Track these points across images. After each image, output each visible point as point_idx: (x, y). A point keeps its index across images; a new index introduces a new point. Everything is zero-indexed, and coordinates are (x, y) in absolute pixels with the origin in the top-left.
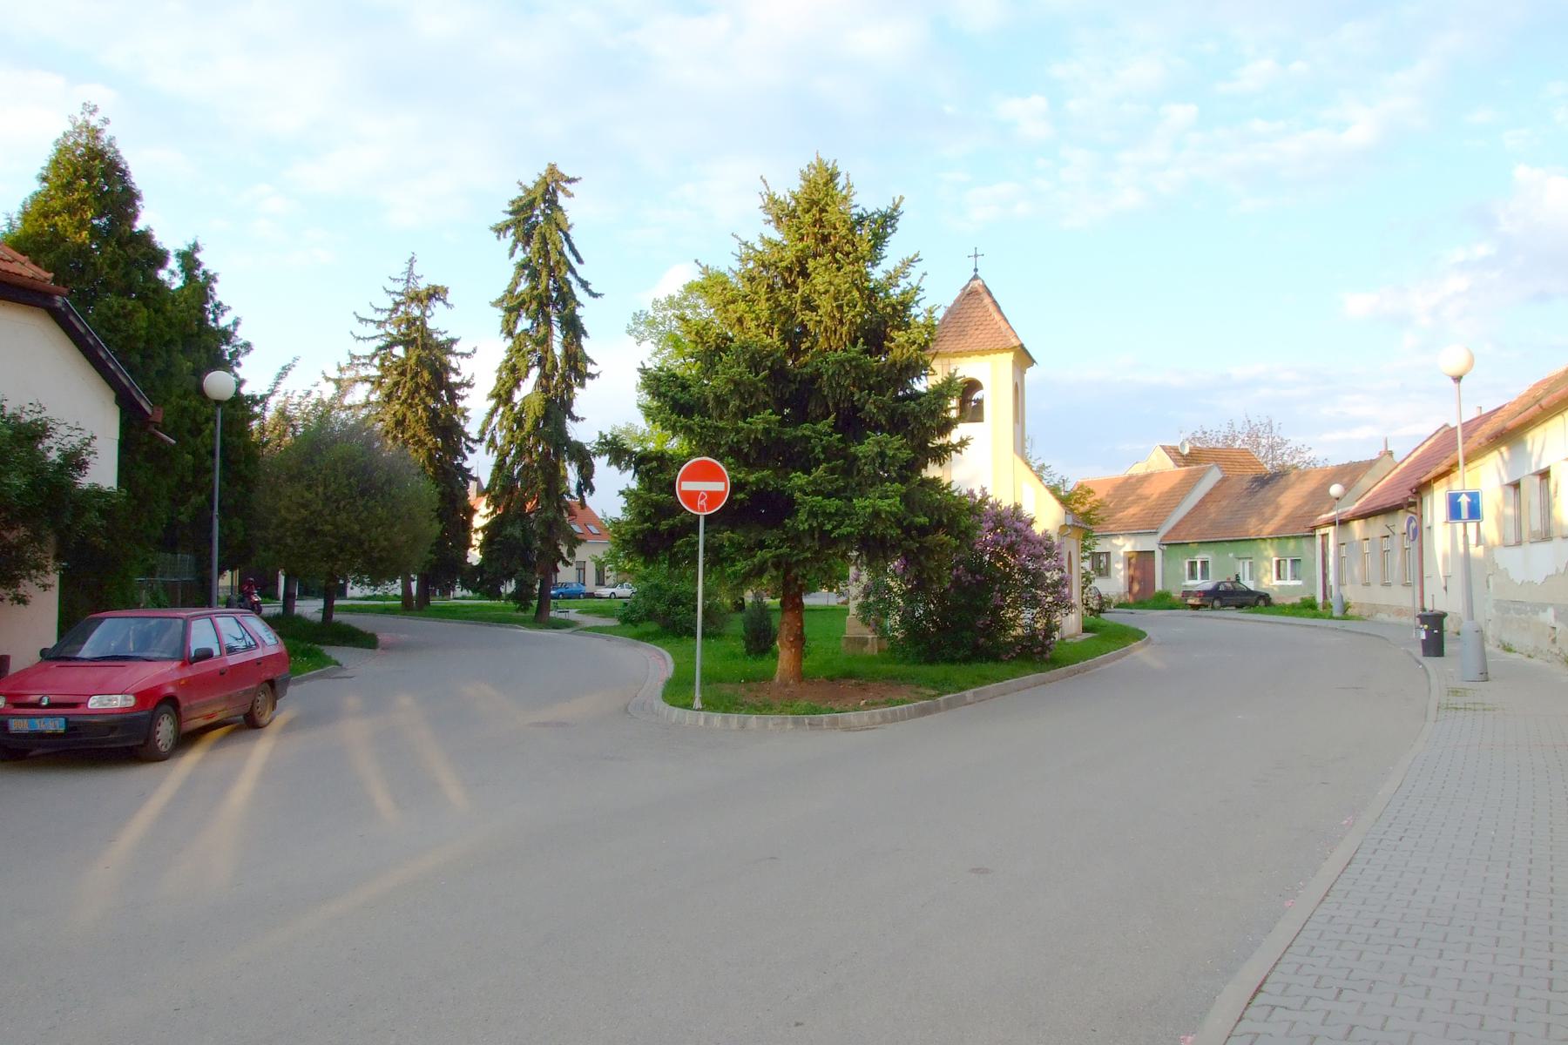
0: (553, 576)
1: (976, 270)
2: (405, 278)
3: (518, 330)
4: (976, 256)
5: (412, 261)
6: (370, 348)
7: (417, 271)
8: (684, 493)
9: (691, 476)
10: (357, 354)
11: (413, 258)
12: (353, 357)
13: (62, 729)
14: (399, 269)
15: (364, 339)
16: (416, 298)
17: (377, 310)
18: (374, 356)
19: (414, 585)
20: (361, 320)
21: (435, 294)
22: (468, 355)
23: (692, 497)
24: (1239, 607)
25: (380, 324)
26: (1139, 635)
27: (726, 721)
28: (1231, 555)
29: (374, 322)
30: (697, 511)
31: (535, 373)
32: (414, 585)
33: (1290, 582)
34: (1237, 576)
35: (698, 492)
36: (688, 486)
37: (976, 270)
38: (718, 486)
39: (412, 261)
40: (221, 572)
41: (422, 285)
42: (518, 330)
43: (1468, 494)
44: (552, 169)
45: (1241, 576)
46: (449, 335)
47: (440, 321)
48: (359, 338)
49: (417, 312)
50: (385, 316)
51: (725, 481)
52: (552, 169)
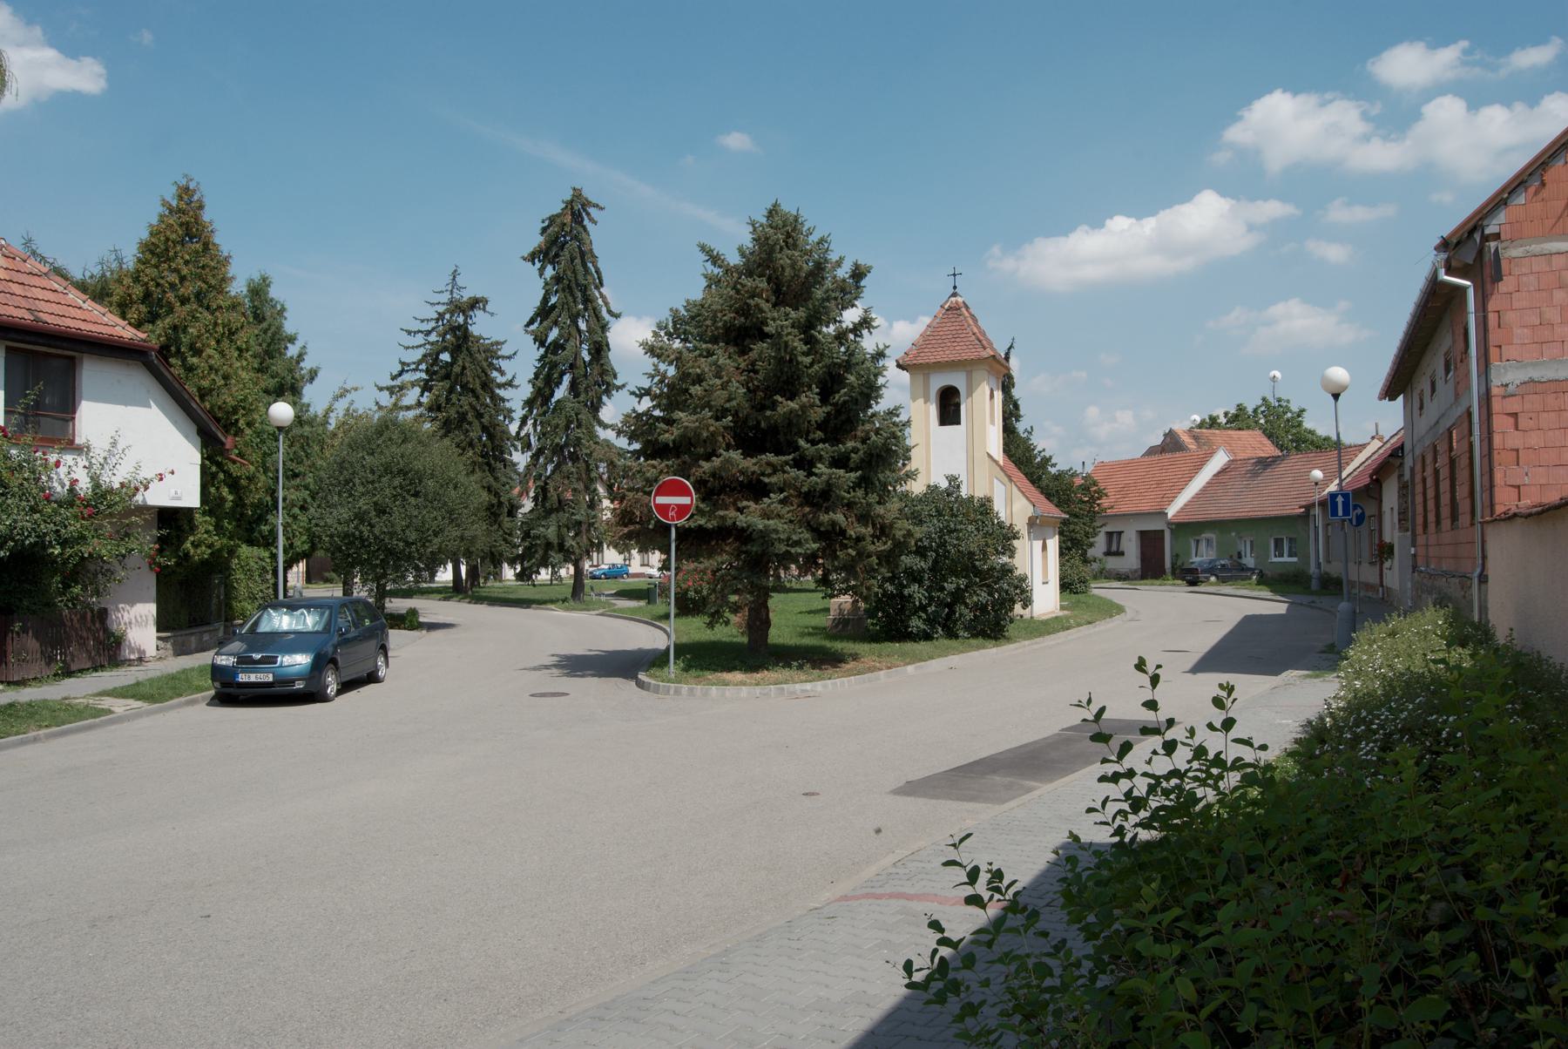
0: (509, 583)
1: (955, 287)
2: (450, 288)
3: (550, 340)
4: (954, 275)
5: (455, 275)
6: (417, 355)
7: (460, 281)
8: (657, 506)
9: (662, 491)
10: (407, 361)
11: (455, 271)
12: (403, 364)
13: (271, 679)
14: (444, 281)
15: (413, 347)
16: (458, 307)
17: (422, 321)
18: (419, 363)
19: (463, 569)
20: (409, 333)
21: (475, 303)
22: (509, 358)
23: (664, 509)
24: (1242, 580)
25: (428, 333)
26: (1120, 609)
27: (825, 686)
28: (1233, 534)
29: (422, 332)
30: (668, 519)
31: (567, 379)
32: (463, 569)
33: (1286, 559)
34: (1239, 553)
35: (670, 505)
36: (661, 500)
37: (955, 287)
38: (686, 500)
39: (455, 275)
40: (288, 565)
41: (466, 295)
42: (550, 340)
43: (1343, 495)
44: (577, 194)
45: (1243, 554)
46: (493, 340)
47: (481, 326)
48: (407, 348)
49: (461, 319)
50: (433, 324)
51: (690, 495)
52: (577, 194)
